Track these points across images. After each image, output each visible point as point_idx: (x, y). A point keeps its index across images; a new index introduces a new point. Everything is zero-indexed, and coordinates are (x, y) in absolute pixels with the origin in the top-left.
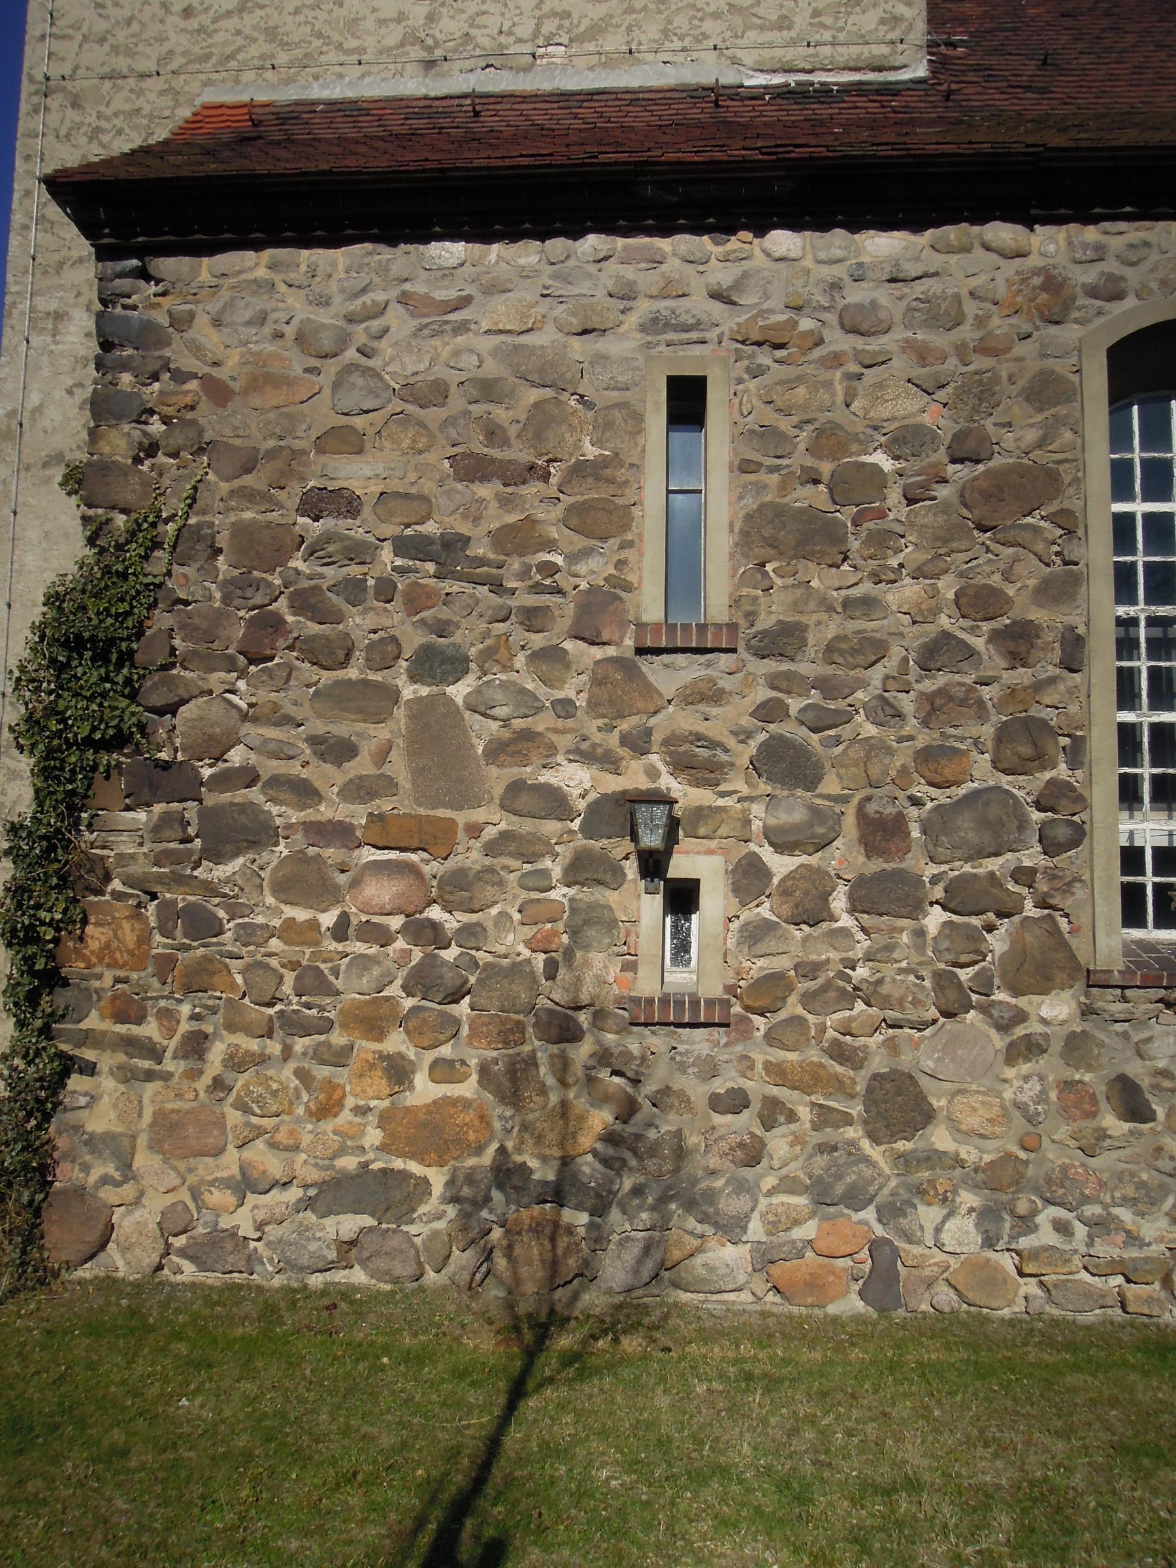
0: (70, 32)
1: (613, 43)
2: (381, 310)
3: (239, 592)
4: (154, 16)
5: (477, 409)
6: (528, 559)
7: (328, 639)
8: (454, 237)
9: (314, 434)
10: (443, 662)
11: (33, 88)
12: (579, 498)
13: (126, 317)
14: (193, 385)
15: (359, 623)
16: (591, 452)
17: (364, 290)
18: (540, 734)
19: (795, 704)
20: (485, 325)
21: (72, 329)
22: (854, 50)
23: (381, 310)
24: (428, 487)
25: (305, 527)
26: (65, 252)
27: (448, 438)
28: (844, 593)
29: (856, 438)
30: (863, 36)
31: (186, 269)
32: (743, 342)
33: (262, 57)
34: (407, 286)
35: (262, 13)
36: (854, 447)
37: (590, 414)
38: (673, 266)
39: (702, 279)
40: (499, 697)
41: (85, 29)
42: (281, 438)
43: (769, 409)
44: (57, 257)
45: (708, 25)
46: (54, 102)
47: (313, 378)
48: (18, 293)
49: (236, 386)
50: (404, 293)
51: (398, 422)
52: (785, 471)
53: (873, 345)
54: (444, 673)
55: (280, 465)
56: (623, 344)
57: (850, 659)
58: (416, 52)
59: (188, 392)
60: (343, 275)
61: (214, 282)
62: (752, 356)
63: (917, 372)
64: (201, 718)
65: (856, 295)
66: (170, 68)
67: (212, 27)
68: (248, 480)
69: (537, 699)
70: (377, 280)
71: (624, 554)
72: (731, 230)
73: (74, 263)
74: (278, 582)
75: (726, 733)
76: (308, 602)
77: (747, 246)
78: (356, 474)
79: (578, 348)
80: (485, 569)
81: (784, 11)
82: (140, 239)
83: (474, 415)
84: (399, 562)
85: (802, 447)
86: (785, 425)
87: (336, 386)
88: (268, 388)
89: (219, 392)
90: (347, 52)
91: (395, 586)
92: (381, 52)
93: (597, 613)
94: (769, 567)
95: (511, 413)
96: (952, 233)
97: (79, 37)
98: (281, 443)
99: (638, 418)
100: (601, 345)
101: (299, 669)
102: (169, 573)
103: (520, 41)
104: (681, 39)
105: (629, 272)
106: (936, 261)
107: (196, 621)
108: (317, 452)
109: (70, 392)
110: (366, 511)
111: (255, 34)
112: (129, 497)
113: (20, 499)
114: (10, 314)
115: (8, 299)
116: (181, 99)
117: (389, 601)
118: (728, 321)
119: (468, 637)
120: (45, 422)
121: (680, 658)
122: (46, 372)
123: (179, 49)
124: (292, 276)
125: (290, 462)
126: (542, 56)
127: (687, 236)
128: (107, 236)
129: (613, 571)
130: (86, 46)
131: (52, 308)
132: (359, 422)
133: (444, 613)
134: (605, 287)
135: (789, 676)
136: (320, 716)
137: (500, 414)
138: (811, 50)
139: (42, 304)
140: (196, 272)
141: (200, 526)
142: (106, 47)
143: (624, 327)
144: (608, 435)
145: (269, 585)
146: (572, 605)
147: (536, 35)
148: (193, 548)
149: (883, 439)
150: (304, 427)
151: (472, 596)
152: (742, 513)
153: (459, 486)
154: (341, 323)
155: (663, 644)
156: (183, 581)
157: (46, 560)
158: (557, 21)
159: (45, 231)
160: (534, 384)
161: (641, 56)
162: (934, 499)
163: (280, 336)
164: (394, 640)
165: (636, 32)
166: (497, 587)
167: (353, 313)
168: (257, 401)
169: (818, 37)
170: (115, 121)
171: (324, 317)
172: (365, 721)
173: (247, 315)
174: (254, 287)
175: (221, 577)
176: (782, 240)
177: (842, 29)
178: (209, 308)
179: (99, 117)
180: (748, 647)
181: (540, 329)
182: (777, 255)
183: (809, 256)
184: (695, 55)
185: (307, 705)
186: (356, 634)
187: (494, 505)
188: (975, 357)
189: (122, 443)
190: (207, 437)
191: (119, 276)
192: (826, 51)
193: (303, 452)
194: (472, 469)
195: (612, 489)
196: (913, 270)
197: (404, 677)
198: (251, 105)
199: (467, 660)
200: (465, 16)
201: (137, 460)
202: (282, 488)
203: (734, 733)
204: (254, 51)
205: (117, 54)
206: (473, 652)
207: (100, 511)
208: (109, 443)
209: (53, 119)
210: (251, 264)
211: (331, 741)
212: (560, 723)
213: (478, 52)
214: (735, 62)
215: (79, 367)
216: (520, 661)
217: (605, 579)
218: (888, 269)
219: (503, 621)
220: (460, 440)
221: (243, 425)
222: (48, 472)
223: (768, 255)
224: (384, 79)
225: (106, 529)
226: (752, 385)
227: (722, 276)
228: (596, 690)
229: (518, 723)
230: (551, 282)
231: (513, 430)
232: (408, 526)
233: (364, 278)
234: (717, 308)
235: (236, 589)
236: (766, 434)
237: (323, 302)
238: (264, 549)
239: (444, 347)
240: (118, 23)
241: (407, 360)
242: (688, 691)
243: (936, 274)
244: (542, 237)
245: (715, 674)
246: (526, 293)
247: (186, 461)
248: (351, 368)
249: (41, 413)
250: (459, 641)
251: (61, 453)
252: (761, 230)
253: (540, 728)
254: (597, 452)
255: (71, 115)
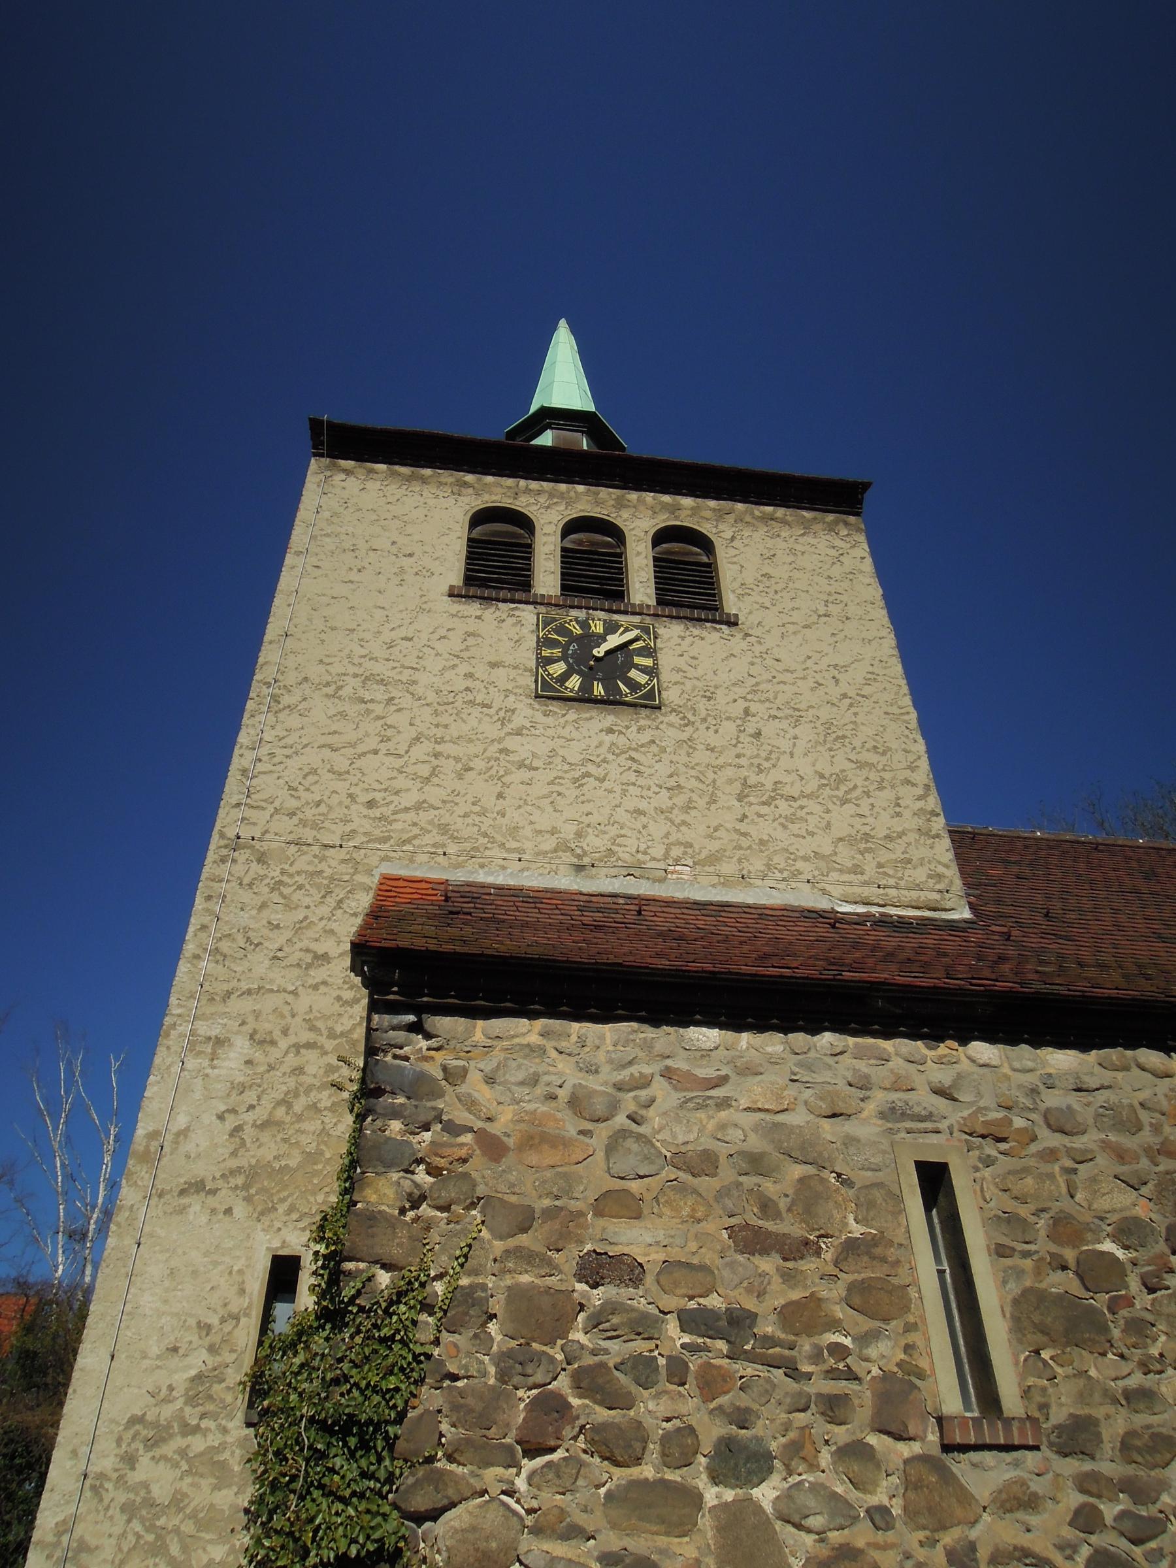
0: (263, 804)
1: (729, 868)
2: (644, 1082)
3: (518, 1367)
4: (340, 803)
5: (749, 1181)
6: (816, 1339)
7: (620, 1429)
8: (710, 1024)
9: (592, 1196)
10: (748, 1460)
11: (223, 842)
12: (856, 1276)
13: (399, 1066)
14: (467, 1138)
15: (653, 1408)
16: (857, 1230)
17: (631, 1063)
18: (860, 1552)
19: (1109, 1511)
20: (744, 1103)
21: (232, 1055)
22: (914, 894)
23: (644, 1082)
24: (708, 1257)
25: (583, 1294)
26: (234, 983)
27: (724, 1209)
28: (1120, 1383)
29: (1087, 1227)
30: (918, 885)
31: (461, 1029)
32: (970, 1134)
33: (434, 845)
34: (669, 1062)
35: (436, 812)
36: (1089, 1236)
37: (851, 1192)
38: (897, 1063)
39: (923, 1076)
40: (811, 1503)
41: (277, 804)
42: (557, 1198)
43: (1006, 1196)
44: (226, 987)
45: (800, 865)
46: (242, 856)
47: (587, 1140)
48: (179, 1016)
49: (511, 1142)
50: (668, 1068)
51: (673, 1188)
52: (1035, 1257)
53: (1079, 1142)
54: (749, 1473)
55: (557, 1227)
56: (866, 1126)
57: (1148, 1458)
58: (568, 858)
59: (462, 1145)
60: (611, 1048)
61: (489, 1042)
62: (980, 1147)
63: (1120, 1169)
64: (474, 1529)
65: (1053, 1100)
66: (351, 844)
67: (392, 817)
68: (523, 1239)
69: (851, 1506)
70: (641, 1054)
71: (912, 1338)
72: (940, 1039)
73: (243, 993)
74: (560, 1357)
75: (1051, 1547)
76: (592, 1382)
77: (954, 1052)
78: (636, 1239)
79: (828, 1128)
80: (777, 1349)
81: (856, 861)
82: (425, 999)
83: (746, 1187)
84: (687, 1339)
85: (1043, 1233)
86: (1024, 1211)
87: (610, 1150)
88: (546, 1147)
89: (493, 1147)
90: (509, 850)
91: (687, 1367)
92: (538, 854)
93: (896, 1403)
94: (1045, 1355)
95: (778, 1187)
96: (1114, 1054)
97: (271, 809)
98: (557, 1203)
99: (898, 1199)
100: (848, 1127)
101: (589, 1465)
102: (437, 1342)
103: (654, 859)
104: (781, 871)
105: (863, 1066)
106: (1107, 1076)
107: (470, 1401)
108: (595, 1215)
109: (221, 1117)
110: (649, 1279)
111: (430, 828)
112: (395, 1252)
113: (147, 1229)
114: (168, 1035)
115: (168, 1020)
116: (360, 868)
117: (683, 1384)
118: (954, 1116)
119: (768, 1430)
120: (189, 1146)
121: (988, 1457)
122: (198, 1095)
123: (361, 830)
124: (563, 1044)
125: (566, 1225)
126: (672, 873)
127: (906, 1041)
128: (394, 993)
129: (903, 1356)
130: (276, 817)
131: (213, 1033)
132: (635, 1186)
133: (744, 1400)
134: (845, 1078)
135: (1094, 1476)
136: (614, 1526)
137: (770, 1187)
138: (881, 891)
139: (203, 1029)
140: (470, 1032)
141: (472, 1287)
142: (295, 820)
143: (865, 1114)
144: (872, 1214)
145: (552, 1360)
146: (868, 1393)
147: (666, 856)
148: (467, 1314)
149: (1109, 1229)
150: (582, 1188)
151: (768, 1380)
152: (1010, 1298)
153: (741, 1258)
154: (610, 1090)
155: (972, 1440)
156: (453, 1351)
157: (166, 1302)
158: (682, 849)
159: (217, 962)
160: (796, 1161)
161: (752, 881)
162: (1168, 1288)
163: (554, 1097)
164: (691, 1430)
165: (745, 864)
166: (793, 1372)
167: (622, 1082)
168: (533, 1158)
169: (884, 882)
170: (297, 878)
171: (592, 1083)
172: (667, 1534)
173: (521, 1076)
174: (527, 1051)
175: (495, 1348)
176: (981, 1050)
177: (901, 879)
178: (481, 1066)
179: (282, 873)
180: (1051, 1445)
181: (794, 1110)
182: (981, 1062)
183: (1006, 1065)
184: (794, 885)
185: (599, 1513)
186: (648, 1422)
187: (776, 1279)
188: (1161, 1159)
189: (390, 1192)
190: (481, 1190)
191: (394, 1028)
192: (893, 892)
193: (581, 1214)
194: (752, 1241)
195: (886, 1268)
196: (1093, 1083)
197: (704, 1477)
198: (446, 882)
199: (769, 1456)
200: (607, 837)
201: (403, 1211)
202: (558, 1251)
203: (1060, 1548)
204: (428, 839)
205: (304, 826)
206: (774, 1446)
207: (362, 1265)
208: (376, 1191)
209: (239, 869)
210: (524, 1030)
211: (627, 1561)
212: (880, 1537)
213: (620, 863)
214: (825, 892)
215: (234, 1093)
216: (825, 1457)
217: (897, 1365)
218: (1072, 1081)
219: (804, 1410)
220: (736, 1211)
221: (521, 1181)
222: (185, 1201)
223: (973, 1061)
224: (541, 875)
225: (369, 1285)
226: (987, 1173)
227: (943, 1076)
228: (911, 1495)
229: (834, 1536)
230: (797, 1070)
231: (783, 1204)
232: (691, 1298)
233: (631, 1052)
234: (941, 1103)
235: (514, 1365)
236: (1009, 1220)
237: (592, 1070)
238: (544, 1317)
239: (710, 1120)
240: (308, 803)
241: (677, 1129)
242: (1004, 1496)
243: (1109, 1087)
244: (786, 1031)
245: (1026, 1475)
246: (775, 1078)
247: (459, 1215)
248: (623, 1133)
249: (186, 1137)
250: (761, 1434)
251: (202, 1182)
252: (964, 1041)
253: (860, 1543)
254: (864, 1230)
255: (256, 868)
